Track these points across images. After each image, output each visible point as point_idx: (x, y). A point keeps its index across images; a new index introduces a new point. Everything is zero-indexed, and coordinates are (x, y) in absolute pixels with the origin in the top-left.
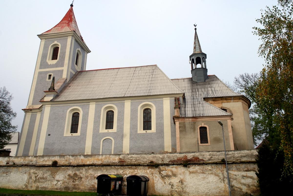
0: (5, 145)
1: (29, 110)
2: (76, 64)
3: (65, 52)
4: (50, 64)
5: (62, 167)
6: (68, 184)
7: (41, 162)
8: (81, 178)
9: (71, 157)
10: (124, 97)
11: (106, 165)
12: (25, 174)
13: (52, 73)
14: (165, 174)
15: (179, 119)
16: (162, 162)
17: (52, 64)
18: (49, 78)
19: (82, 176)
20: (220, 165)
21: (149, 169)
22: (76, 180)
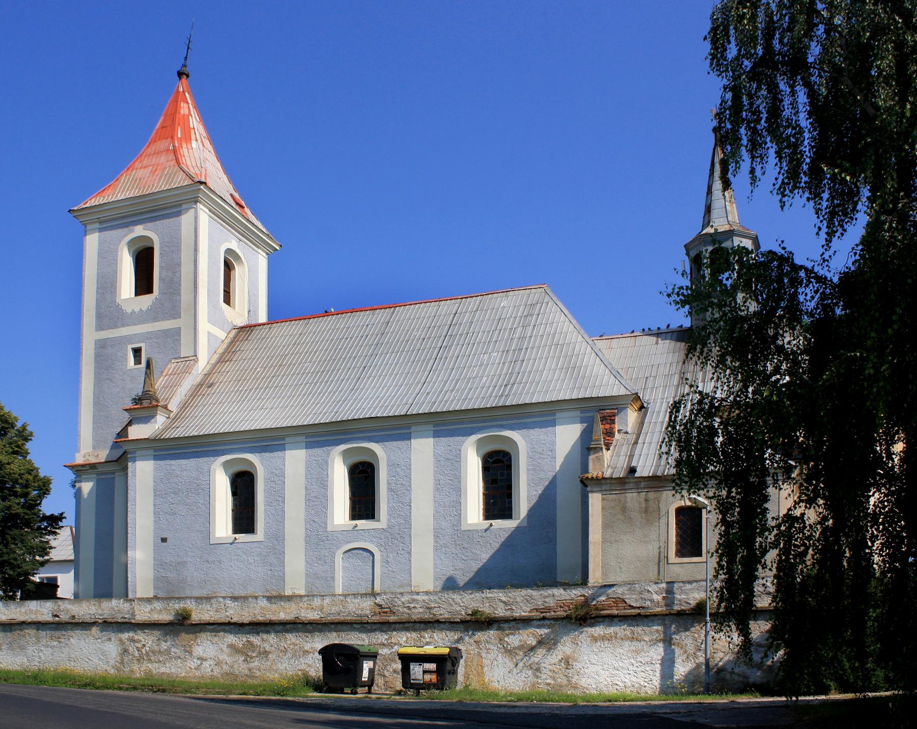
0: (737, 626)
1: (87, 468)
2: (227, 300)
3: (179, 265)
4: (129, 311)
5: (208, 627)
6: (232, 667)
7: (143, 614)
8: (266, 653)
9: (228, 602)
10: (406, 415)
11: (335, 621)
12: (108, 642)
13: (143, 342)
14: (517, 644)
15: (602, 484)
16: (508, 613)
17: (137, 310)
18: (138, 360)
19: (267, 649)
20: (690, 618)
21: (468, 632)
22: (251, 657)
